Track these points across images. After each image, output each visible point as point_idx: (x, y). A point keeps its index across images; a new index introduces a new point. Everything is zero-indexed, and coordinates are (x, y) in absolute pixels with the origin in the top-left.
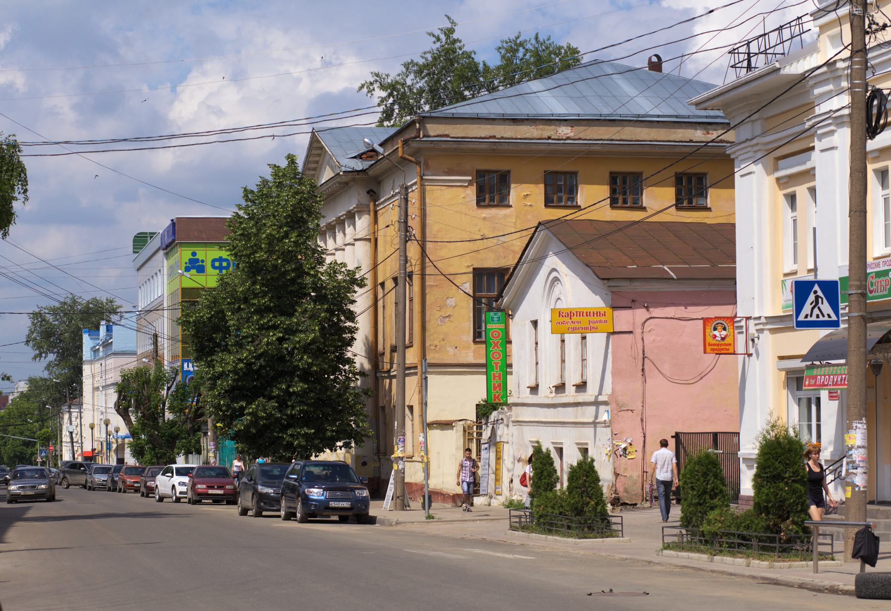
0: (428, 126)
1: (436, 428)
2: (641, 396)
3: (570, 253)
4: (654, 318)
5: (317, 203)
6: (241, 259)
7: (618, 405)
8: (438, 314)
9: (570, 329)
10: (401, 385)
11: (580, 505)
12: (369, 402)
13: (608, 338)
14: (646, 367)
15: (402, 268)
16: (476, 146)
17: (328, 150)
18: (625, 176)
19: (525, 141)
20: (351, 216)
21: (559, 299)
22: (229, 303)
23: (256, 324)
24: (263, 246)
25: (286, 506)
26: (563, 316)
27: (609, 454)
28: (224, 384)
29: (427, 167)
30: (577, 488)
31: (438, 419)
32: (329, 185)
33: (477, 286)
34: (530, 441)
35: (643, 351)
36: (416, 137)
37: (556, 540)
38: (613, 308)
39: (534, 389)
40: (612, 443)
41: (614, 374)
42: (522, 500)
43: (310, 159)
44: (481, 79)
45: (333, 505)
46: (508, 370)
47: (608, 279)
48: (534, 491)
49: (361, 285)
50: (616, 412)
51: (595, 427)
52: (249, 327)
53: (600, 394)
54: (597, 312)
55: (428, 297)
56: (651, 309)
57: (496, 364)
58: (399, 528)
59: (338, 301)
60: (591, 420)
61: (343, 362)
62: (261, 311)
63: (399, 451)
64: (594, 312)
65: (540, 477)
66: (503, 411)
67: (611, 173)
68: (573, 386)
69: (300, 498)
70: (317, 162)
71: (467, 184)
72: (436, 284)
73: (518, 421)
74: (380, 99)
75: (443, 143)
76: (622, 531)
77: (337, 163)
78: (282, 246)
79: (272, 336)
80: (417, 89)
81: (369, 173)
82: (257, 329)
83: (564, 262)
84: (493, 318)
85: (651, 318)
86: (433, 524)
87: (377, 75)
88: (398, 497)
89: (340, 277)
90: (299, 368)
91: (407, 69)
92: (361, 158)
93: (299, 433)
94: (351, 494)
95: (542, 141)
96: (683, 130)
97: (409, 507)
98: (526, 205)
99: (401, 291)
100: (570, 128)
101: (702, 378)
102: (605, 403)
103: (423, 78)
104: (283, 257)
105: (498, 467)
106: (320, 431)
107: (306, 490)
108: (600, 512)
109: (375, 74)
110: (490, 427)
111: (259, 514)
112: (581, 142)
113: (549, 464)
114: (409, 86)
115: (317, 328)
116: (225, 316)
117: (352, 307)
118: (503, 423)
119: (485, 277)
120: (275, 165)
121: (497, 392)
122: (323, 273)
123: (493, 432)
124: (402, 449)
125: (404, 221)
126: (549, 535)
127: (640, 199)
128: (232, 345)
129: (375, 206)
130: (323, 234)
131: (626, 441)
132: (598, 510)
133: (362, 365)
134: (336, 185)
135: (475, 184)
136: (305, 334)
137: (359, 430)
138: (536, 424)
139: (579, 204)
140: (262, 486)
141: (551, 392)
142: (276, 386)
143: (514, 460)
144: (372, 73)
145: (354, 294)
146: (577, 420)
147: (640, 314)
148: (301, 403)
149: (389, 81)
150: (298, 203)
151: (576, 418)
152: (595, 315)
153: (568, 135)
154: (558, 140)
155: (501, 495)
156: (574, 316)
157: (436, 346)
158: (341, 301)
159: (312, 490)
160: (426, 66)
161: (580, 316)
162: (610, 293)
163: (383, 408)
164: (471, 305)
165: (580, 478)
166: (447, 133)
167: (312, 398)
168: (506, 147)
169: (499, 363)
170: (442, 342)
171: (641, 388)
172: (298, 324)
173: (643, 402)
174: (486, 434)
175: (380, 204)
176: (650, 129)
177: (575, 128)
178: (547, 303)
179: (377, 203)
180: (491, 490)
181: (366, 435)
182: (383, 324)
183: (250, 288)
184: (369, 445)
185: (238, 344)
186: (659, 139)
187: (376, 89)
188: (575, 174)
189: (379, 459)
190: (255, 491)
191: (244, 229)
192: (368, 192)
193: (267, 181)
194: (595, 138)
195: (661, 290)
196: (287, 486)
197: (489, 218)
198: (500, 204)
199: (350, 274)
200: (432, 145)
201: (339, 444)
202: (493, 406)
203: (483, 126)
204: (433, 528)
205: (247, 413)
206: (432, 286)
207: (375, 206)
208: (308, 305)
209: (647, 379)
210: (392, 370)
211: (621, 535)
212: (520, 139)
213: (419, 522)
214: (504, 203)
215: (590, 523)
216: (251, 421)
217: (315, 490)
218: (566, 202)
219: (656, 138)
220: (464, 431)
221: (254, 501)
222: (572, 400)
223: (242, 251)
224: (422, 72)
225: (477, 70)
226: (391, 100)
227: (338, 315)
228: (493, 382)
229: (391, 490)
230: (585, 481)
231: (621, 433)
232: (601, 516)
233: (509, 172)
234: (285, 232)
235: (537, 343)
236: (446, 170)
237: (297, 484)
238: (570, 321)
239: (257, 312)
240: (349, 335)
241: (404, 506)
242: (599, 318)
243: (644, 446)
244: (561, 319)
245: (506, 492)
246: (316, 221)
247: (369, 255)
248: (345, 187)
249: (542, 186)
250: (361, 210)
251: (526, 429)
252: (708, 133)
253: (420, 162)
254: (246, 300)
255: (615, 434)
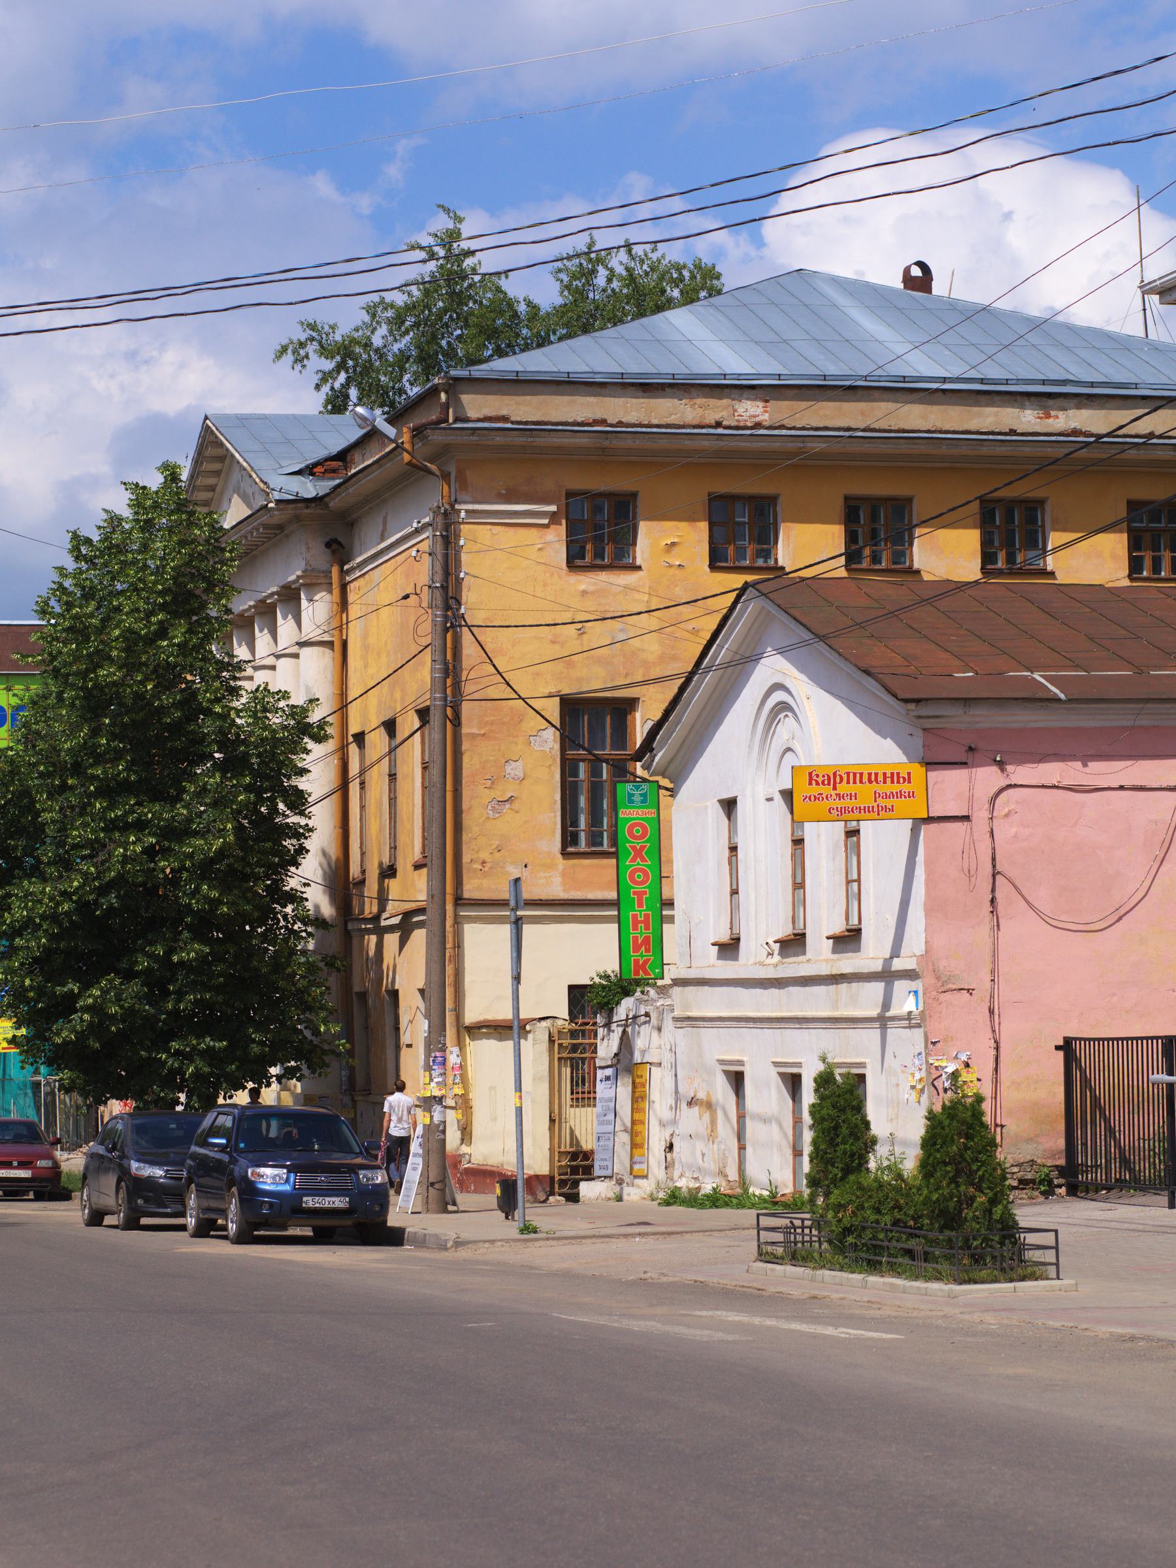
0: (465, 398)
1: (487, 1036)
2: (988, 958)
3: (821, 646)
4: (1016, 786)
5: (226, 565)
6: (67, 680)
7: (938, 978)
8: (486, 796)
9: (834, 812)
10: (436, 940)
11: (952, 1205)
12: (333, 980)
13: (915, 832)
14: (999, 894)
15: (439, 686)
16: (566, 440)
17: (241, 460)
18: (875, 503)
19: (669, 431)
20: (290, 597)
21: (789, 749)
22: (42, 775)
23: (100, 819)
24: (114, 653)
25: (199, 1207)
26: (817, 784)
27: (919, 1087)
28: (34, 944)
29: (463, 484)
30: (946, 1164)
31: (490, 1017)
32: (243, 532)
33: (568, 739)
34: (718, 1061)
35: (994, 859)
36: (439, 422)
37: (892, 1285)
38: (927, 764)
39: (729, 948)
40: (927, 1061)
41: (930, 910)
42: (699, 1189)
43: (198, 482)
44: (525, 331)
45: (311, 1204)
46: (664, 913)
47: (917, 701)
48: (818, 1172)
49: (319, 739)
50: (934, 993)
51: (884, 1028)
52: (85, 825)
53: (896, 953)
54: (892, 774)
55: (466, 760)
56: (1010, 768)
57: (640, 895)
58: (463, 1253)
59: (272, 770)
60: (874, 1012)
61: (280, 898)
62: (111, 791)
63: (433, 1084)
64: (885, 774)
65: (832, 1140)
66: (646, 998)
67: (847, 498)
68: (828, 938)
69: (234, 1189)
70: (212, 488)
71: (546, 521)
72: (482, 732)
73: (689, 1019)
74: (320, 375)
75: (500, 433)
76: (1057, 1265)
77: (262, 485)
78: (154, 655)
79: (134, 843)
80: (394, 355)
81: (331, 504)
82: (103, 830)
83: (802, 669)
84: (631, 796)
85: (1010, 786)
86: (537, 1244)
87: (313, 327)
88: (432, 1184)
89: (276, 720)
90: (191, 910)
91: (374, 316)
92: (312, 474)
93: (194, 1048)
94: (346, 1180)
95: (704, 431)
96: (996, 409)
97: (454, 1204)
98: (670, 566)
99: (437, 736)
100: (761, 404)
101: (1120, 918)
102: (910, 975)
103: (407, 332)
104: (157, 677)
105: (637, 1116)
106: (239, 1042)
107: (250, 1171)
108: (1001, 1221)
109: (309, 325)
110: (617, 1032)
111: (132, 1224)
112: (784, 432)
113: (853, 1108)
114: (377, 350)
115: (229, 826)
116: (33, 802)
117: (302, 783)
118: (649, 1022)
119: (586, 717)
120: (137, 485)
121: (642, 956)
122: (241, 711)
123: (626, 1043)
124: (440, 1079)
125: (442, 586)
126: (870, 1274)
127: (908, 552)
128: (49, 864)
129: (343, 573)
130: (245, 624)
131: (956, 1057)
132: (996, 1217)
133: (317, 907)
134: (258, 530)
135: (564, 522)
136: (205, 840)
137: (316, 1041)
138: (734, 1024)
139: (780, 563)
140: (139, 1161)
141: (770, 954)
142: (142, 950)
143: (677, 1100)
144: (302, 323)
145: (304, 756)
146: (837, 1014)
147: (987, 777)
148: (194, 986)
149: (338, 338)
150: (188, 564)
151: (836, 1008)
152: (889, 780)
153: (757, 419)
154: (737, 428)
155: (646, 1177)
156: (841, 782)
157: (484, 862)
158: (280, 769)
159: (262, 1170)
160: (409, 308)
161: (855, 782)
162: (921, 733)
163: (363, 996)
164: (558, 776)
165: (953, 1141)
166: (504, 412)
167: (220, 975)
168: (630, 443)
169: (645, 893)
170: (497, 855)
171: (989, 941)
172: (189, 820)
173: (993, 972)
174: (607, 1047)
175: (353, 569)
176: (928, 408)
177: (772, 403)
178: (760, 759)
179: (346, 567)
180: (621, 1165)
181: (333, 1052)
182: (361, 819)
183: (85, 743)
184: (336, 1072)
185: (60, 859)
186: (947, 427)
187: (311, 355)
188: (773, 500)
189: (354, 1102)
190: (124, 1174)
191: (76, 617)
192: (328, 545)
193: (120, 519)
194: (814, 425)
195: (1033, 725)
196: (202, 1162)
197: (592, 593)
198: (616, 563)
199: (298, 713)
200: (475, 438)
201: (274, 1071)
202: (622, 987)
203: (580, 399)
204: (537, 1253)
205: (81, 1007)
206: (473, 736)
207: (343, 573)
208: (210, 777)
209: (1001, 920)
210: (384, 915)
211: (1053, 1274)
212: (658, 426)
213: (507, 1241)
214: (625, 561)
215: (976, 1248)
216: (91, 1023)
217: (268, 1171)
218: (753, 560)
219: (940, 425)
220: (551, 1041)
221: (121, 1196)
222: (824, 970)
223: (71, 664)
224: (403, 322)
225: (516, 315)
226: (342, 377)
227: (273, 800)
228: (632, 934)
229: (415, 1169)
230: (966, 1148)
231: (945, 1040)
232: (1002, 1230)
233: (634, 495)
234: (161, 622)
235: (733, 849)
236: (504, 492)
237: (226, 1158)
238: (833, 793)
239: (99, 794)
240: (294, 841)
241: (445, 1204)
242: (896, 788)
243: (996, 1069)
244: (814, 790)
245: (657, 1171)
246: (224, 601)
247: (329, 676)
248: (276, 535)
249: (703, 526)
250: (313, 582)
251: (708, 1035)
252: (1048, 416)
253: (449, 474)
254: (77, 769)
255: (934, 1043)
